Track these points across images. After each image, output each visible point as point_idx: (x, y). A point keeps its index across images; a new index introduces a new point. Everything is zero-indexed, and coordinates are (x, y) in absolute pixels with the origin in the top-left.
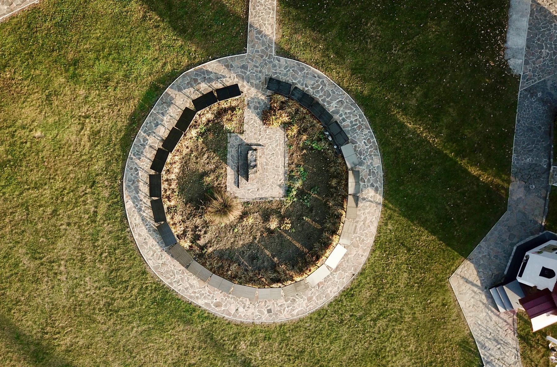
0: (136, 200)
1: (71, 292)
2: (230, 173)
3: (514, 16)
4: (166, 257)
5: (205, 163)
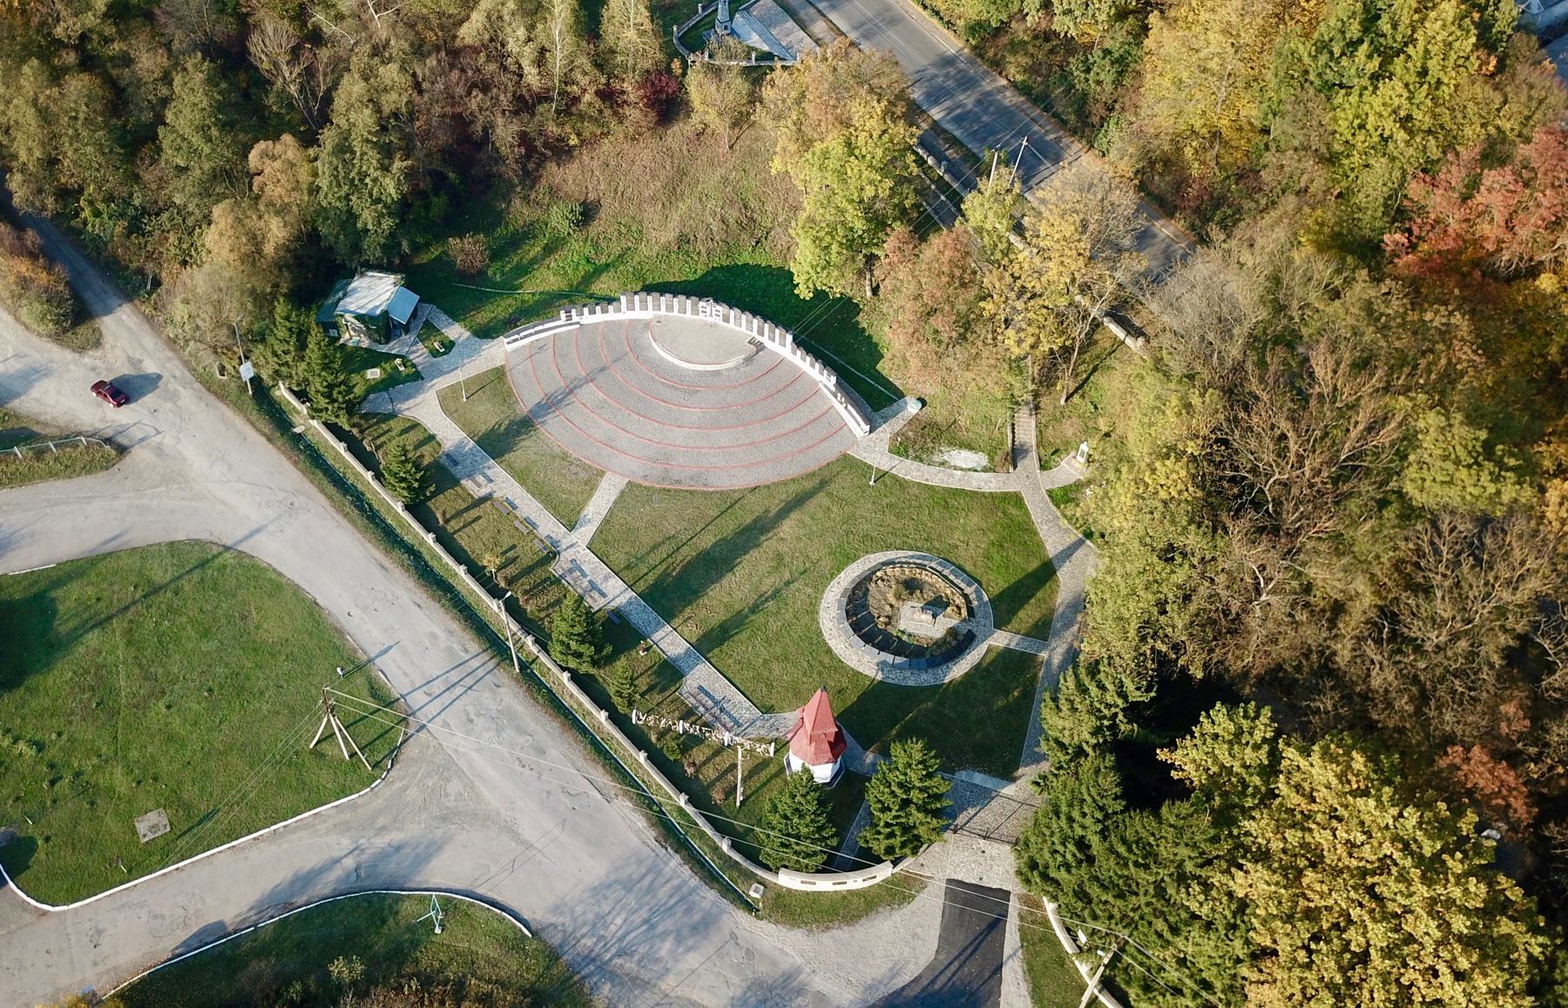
3: (995, 780)
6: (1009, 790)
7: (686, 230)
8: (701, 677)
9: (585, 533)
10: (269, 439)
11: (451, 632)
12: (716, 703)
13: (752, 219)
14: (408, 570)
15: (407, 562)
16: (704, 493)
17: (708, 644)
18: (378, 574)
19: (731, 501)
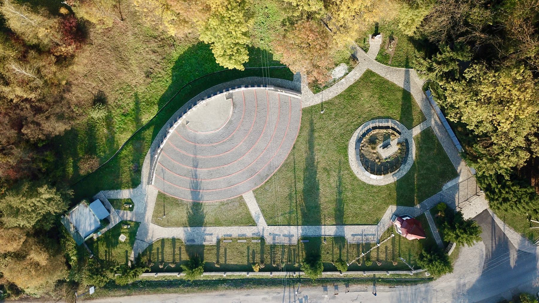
0: (362, 129)
1: (333, 128)
2: (381, 144)
3: (454, 180)
4: (354, 143)
5: (380, 138)
6: (461, 179)
7: (145, 69)
8: (351, 233)
9: (262, 222)
10: (128, 295)
11: (267, 293)
12: (362, 235)
13: (162, 39)
14: (230, 289)
15: (226, 287)
16: (279, 171)
17: (340, 219)
18: (224, 298)
19: (289, 165)
